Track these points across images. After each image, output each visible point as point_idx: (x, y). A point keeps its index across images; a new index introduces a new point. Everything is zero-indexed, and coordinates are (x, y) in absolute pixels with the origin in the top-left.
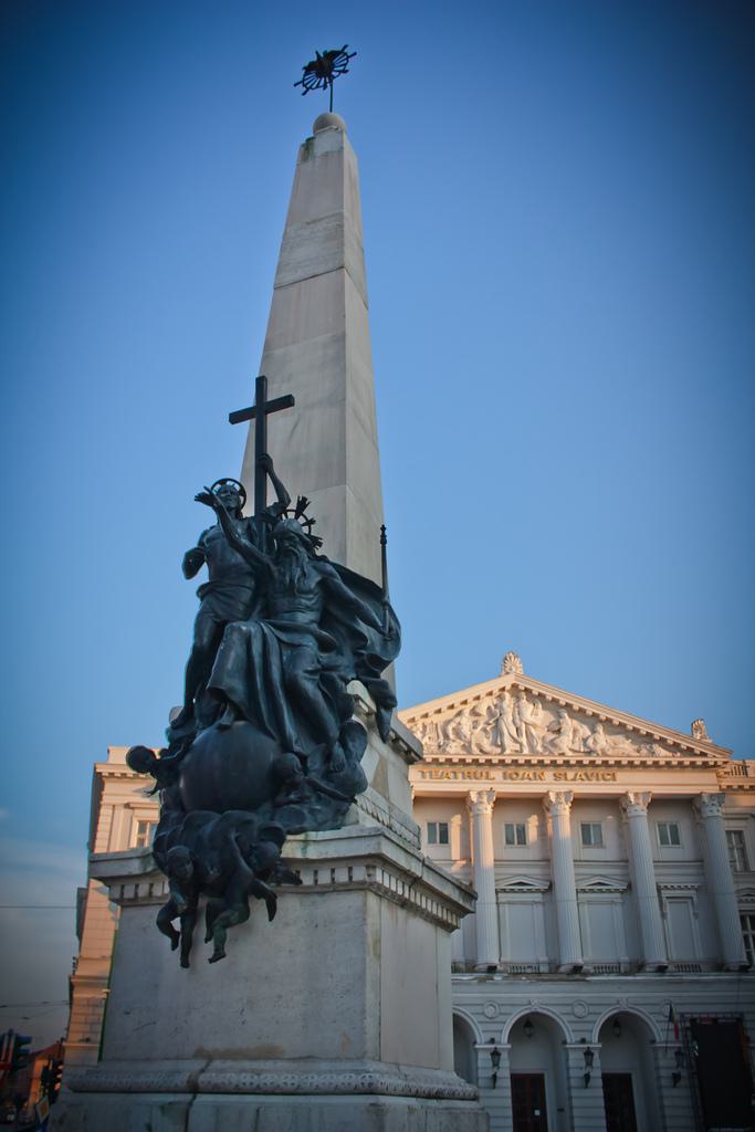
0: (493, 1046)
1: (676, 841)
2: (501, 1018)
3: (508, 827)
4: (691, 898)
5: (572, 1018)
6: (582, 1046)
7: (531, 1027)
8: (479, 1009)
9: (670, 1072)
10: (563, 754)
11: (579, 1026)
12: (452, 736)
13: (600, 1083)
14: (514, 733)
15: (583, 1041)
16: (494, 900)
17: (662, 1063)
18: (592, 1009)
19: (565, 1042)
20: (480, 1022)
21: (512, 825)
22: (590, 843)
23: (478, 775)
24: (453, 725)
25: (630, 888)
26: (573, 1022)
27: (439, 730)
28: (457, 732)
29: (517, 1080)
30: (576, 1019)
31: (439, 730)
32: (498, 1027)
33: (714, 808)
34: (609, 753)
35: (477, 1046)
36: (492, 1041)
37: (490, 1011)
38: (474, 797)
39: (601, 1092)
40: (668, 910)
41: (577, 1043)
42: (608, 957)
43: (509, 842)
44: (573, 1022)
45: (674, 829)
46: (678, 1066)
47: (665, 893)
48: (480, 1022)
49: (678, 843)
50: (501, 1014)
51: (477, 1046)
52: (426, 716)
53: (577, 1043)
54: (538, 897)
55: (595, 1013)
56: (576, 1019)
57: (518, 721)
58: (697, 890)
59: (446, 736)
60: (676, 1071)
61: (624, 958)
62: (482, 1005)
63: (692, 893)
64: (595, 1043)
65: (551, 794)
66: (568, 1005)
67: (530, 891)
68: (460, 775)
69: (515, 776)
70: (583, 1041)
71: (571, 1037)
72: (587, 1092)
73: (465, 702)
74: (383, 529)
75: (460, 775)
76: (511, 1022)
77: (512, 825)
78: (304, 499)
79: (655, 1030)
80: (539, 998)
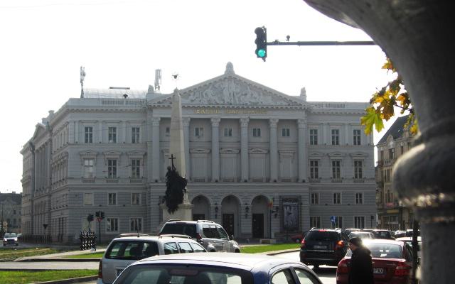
1: (288, 135)
67: (203, 153)
76: (222, 198)
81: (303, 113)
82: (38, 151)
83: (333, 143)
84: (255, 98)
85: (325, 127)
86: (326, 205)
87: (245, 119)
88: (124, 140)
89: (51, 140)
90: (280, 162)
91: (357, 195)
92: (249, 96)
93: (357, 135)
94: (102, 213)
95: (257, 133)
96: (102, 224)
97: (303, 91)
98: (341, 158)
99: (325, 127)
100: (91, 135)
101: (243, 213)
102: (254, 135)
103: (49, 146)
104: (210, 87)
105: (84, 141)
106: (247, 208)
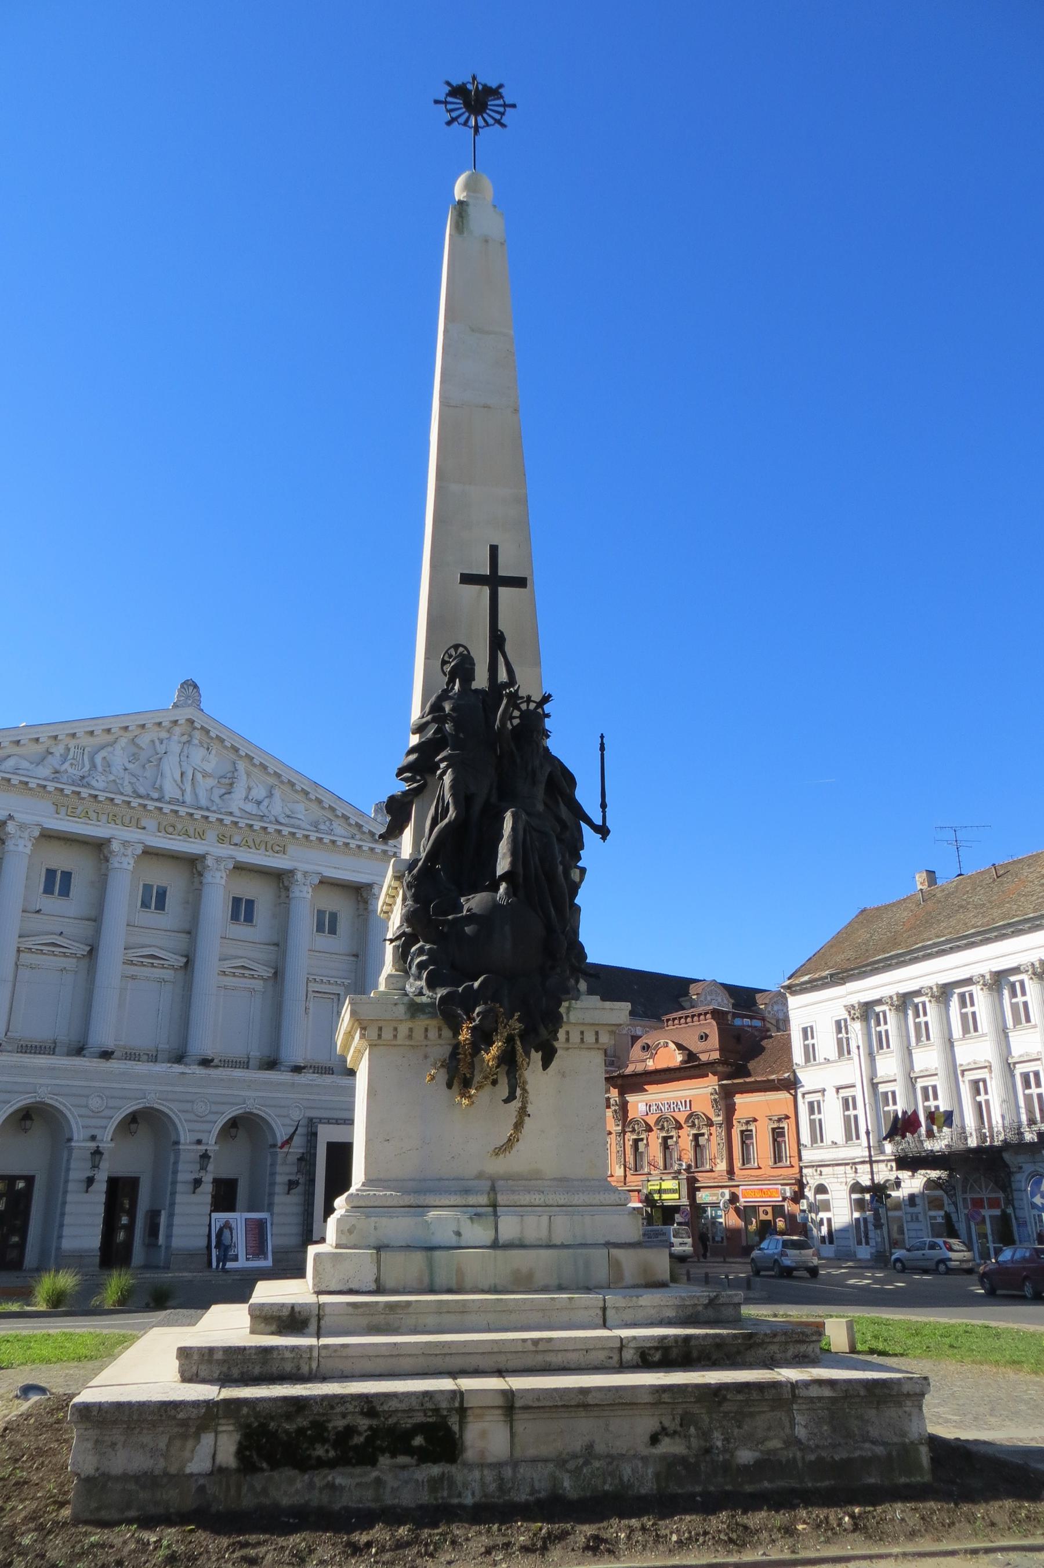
1: (333, 931)
2: (212, 1117)
3: (147, 888)
4: (339, 994)
6: (195, 1147)
7: (144, 1122)
9: (286, 1179)
10: (231, 814)
12: (100, 768)
13: (104, 1187)
14: (178, 777)
15: (93, 1138)
16: (13, 959)
17: (279, 1169)
18: (214, 1108)
19: (177, 1143)
20: (80, 1116)
21: (151, 886)
23: (127, 820)
24: (103, 753)
26: (190, 1121)
27: (86, 757)
29: (217, 1182)
30: (91, 1114)
31: (86, 757)
34: (282, 821)
35: (73, 1144)
36: (93, 1138)
37: (95, 1103)
38: (115, 846)
39: (102, 1198)
41: (191, 1143)
42: (237, 1051)
43: (145, 905)
44: (190, 1121)
45: (334, 917)
46: (298, 1171)
47: (313, 987)
48: (80, 1116)
49: (335, 934)
50: (211, 1112)
51: (73, 1144)
52: (74, 735)
53: (191, 1143)
54: (70, 963)
55: (216, 1113)
56: (195, 1118)
57: (184, 764)
59: (94, 766)
60: (293, 1178)
62: (87, 1096)
64: (211, 1143)
65: (209, 857)
66: (188, 1101)
69: (171, 829)
71: (186, 1137)
72: (194, 1198)
73: (126, 728)
74: (602, 737)
75: (104, 818)
76: (119, 1116)
77: (151, 886)
78: (550, 696)
79: (74, 1126)
80: (47, 1086)
84: (259, 803)
87: (125, 843)
92: (239, 792)
104: (123, 742)
106: (97, 1153)
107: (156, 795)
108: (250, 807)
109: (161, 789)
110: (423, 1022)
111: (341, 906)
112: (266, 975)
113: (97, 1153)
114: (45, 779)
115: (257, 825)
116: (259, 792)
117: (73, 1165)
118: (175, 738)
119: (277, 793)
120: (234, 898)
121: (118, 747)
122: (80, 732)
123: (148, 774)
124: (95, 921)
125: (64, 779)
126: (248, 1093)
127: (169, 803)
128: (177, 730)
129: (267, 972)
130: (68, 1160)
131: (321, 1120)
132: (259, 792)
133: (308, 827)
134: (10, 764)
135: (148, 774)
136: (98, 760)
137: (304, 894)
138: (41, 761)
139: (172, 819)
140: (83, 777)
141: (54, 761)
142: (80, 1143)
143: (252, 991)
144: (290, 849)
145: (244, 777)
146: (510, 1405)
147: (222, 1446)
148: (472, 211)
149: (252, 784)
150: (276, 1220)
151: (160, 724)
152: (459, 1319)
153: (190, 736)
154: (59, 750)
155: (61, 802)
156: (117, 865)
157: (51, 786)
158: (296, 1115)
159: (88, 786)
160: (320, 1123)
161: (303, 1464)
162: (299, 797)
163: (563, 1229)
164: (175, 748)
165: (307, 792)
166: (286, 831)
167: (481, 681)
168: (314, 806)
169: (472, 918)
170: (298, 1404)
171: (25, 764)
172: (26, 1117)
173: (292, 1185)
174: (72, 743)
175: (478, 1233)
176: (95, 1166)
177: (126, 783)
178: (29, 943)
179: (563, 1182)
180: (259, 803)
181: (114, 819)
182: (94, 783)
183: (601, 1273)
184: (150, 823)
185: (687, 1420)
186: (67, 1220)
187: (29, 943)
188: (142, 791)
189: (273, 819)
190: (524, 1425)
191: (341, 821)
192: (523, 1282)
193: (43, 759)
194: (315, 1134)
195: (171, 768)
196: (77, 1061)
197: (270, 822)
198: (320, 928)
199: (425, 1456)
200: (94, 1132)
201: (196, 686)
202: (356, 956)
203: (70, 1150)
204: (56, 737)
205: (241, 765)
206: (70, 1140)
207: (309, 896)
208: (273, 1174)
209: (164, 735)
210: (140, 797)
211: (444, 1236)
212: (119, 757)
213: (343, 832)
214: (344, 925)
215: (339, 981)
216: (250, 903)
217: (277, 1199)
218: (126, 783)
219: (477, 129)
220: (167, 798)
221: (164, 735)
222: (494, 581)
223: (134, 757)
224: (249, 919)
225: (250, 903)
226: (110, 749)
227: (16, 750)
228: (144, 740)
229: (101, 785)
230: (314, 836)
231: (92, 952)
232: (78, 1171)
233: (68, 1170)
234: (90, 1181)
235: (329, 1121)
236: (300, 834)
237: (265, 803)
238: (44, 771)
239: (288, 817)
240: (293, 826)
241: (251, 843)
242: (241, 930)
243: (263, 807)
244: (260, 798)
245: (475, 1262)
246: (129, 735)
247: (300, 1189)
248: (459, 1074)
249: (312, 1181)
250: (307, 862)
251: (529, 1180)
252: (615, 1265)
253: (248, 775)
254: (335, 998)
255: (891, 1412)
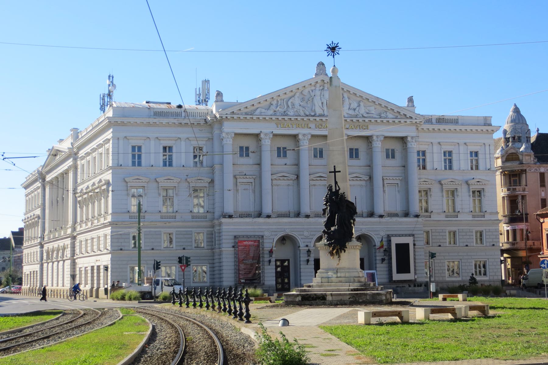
0: (307, 248)
1: (393, 157)
5: (303, 237)
8: (302, 233)
11: (304, 240)
12: (290, 107)
13: (313, 263)
17: (377, 254)
22: (353, 157)
24: (291, 100)
25: (371, 178)
28: (293, 105)
32: (310, 240)
33: (413, 144)
34: (365, 115)
36: (307, 246)
37: (306, 233)
38: (300, 137)
40: (386, 189)
43: (315, 156)
45: (393, 151)
52: (279, 96)
54: (290, 182)
58: (401, 180)
59: (288, 106)
61: (292, 210)
63: (398, 182)
67: (173, 182)
68: (294, 126)
70: (307, 246)
71: (302, 245)
72: (269, 267)
75: (294, 126)
81: (414, 128)
82: (51, 182)
83: (445, 166)
84: (355, 110)
85: (183, 143)
86: (440, 246)
87: (304, 135)
88: (488, 167)
89: (75, 167)
90: (237, 190)
91: (476, 232)
93: (421, 157)
94: (187, 258)
95: (281, 152)
96: (185, 273)
97: (411, 100)
98: (429, 186)
99: (152, 142)
100: (140, 157)
101: (304, 257)
102: (279, 156)
103: (71, 175)
104: (298, 94)
105: (130, 163)
106: (309, 251)
107: (313, 114)
108: (351, 112)
109: (315, 111)
110: (327, 247)
111: (397, 146)
112: (366, 179)
113: (309, 251)
114: (271, 115)
115: (355, 120)
116: (354, 105)
117: (301, 256)
118: (318, 89)
119: (362, 104)
120: (350, 149)
121: (296, 96)
122: (281, 94)
123: (309, 105)
124: (297, 165)
125: (278, 114)
126: (363, 227)
127: (318, 116)
128: (318, 85)
129: (367, 178)
130: (300, 254)
131: (393, 235)
132: (354, 105)
133: (377, 117)
134: (258, 111)
135: (309, 105)
136: (289, 104)
137: (378, 145)
138: (268, 109)
139: (320, 122)
140: (285, 112)
141: (273, 107)
142: (303, 248)
143: (361, 186)
144: (370, 127)
145: (347, 100)
146: (331, 295)
147: (299, 298)
148: (333, 79)
149: (351, 102)
150: (378, 273)
151: (311, 84)
152: (330, 286)
153: (323, 86)
154: (274, 103)
155: (278, 123)
156: (302, 144)
157: (274, 118)
158: (383, 234)
159: (287, 115)
160: (392, 236)
161: (309, 300)
162: (372, 104)
163: (347, 275)
164: (318, 93)
165: (376, 102)
166: (367, 120)
167: (334, 190)
168: (378, 107)
169: (332, 231)
170: (307, 294)
171: (263, 110)
172: (284, 239)
173: (383, 260)
174: (279, 99)
175: (335, 276)
176: (309, 256)
177: (301, 111)
178: (275, 177)
179: (349, 269)
180: (355, 110)
181: (298, 126)
182: (289, 113)
183: (352, 281)
184: (312, 125)
185: (353, 297)
186: (302, 274)
187: (275, 177)
188: (307, 113)
189: (361, 116)
190: (333, 297)
191: (391, 112)
192: (340, 282)
193: (270, 107)
194: (390, 241)
195: (317, 101)
196: (298, 219)
197: (360, 117)
198: (388, 157)
199: (322, 300)
200: (307, 244)
201: (323, 64)
202: (404, 167)
203: (300, 250)
204: (273, 98)
205: (346, 95)
206: (299, 247)
207: (380, 145)
208: (376, 256)
209: (313, 88)
210: (307, 116)
211: (330, 276)
212: (297, 101)
213: (392, 116)
214: (397, 154)
215: (397, 178)
216: (357, 150)
217: (378, 265)
218: (301, 111)
219: (334, 56)
220: (317, 114)
221: (313, 88)
222: (335, 172)
223: (303, 100)
224: (357, 156)
225: (357, 150)
226: (293, 98)
227: (260, 105)
228: (306, 92)
229: (292, 114)
230: (379, 120)
231: (298, 177)
232: (304, 257)
233: (300, 257)
234: (308, 261)
235: (396, 236)
236: (373, 120)
237: (357, 109)
238: (271, 112)
239: (368, 113)
240: (370, 117)
241: (353, 127)
242: (355, 162)
243: (356, 111)
244: (355, 107)
245: (334, 279)
246: (300, 91)
247: (386, 262)
248: (331, 254)
249: (390, 259)
250: (377, 131)
251: (340, 268)
252: (354, 280)
253: (349, 98)
254: (396, 185)
255: (380, 296)
